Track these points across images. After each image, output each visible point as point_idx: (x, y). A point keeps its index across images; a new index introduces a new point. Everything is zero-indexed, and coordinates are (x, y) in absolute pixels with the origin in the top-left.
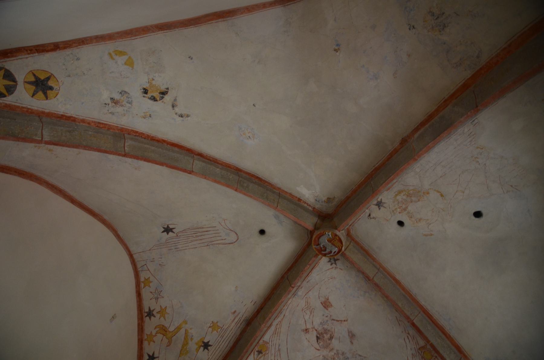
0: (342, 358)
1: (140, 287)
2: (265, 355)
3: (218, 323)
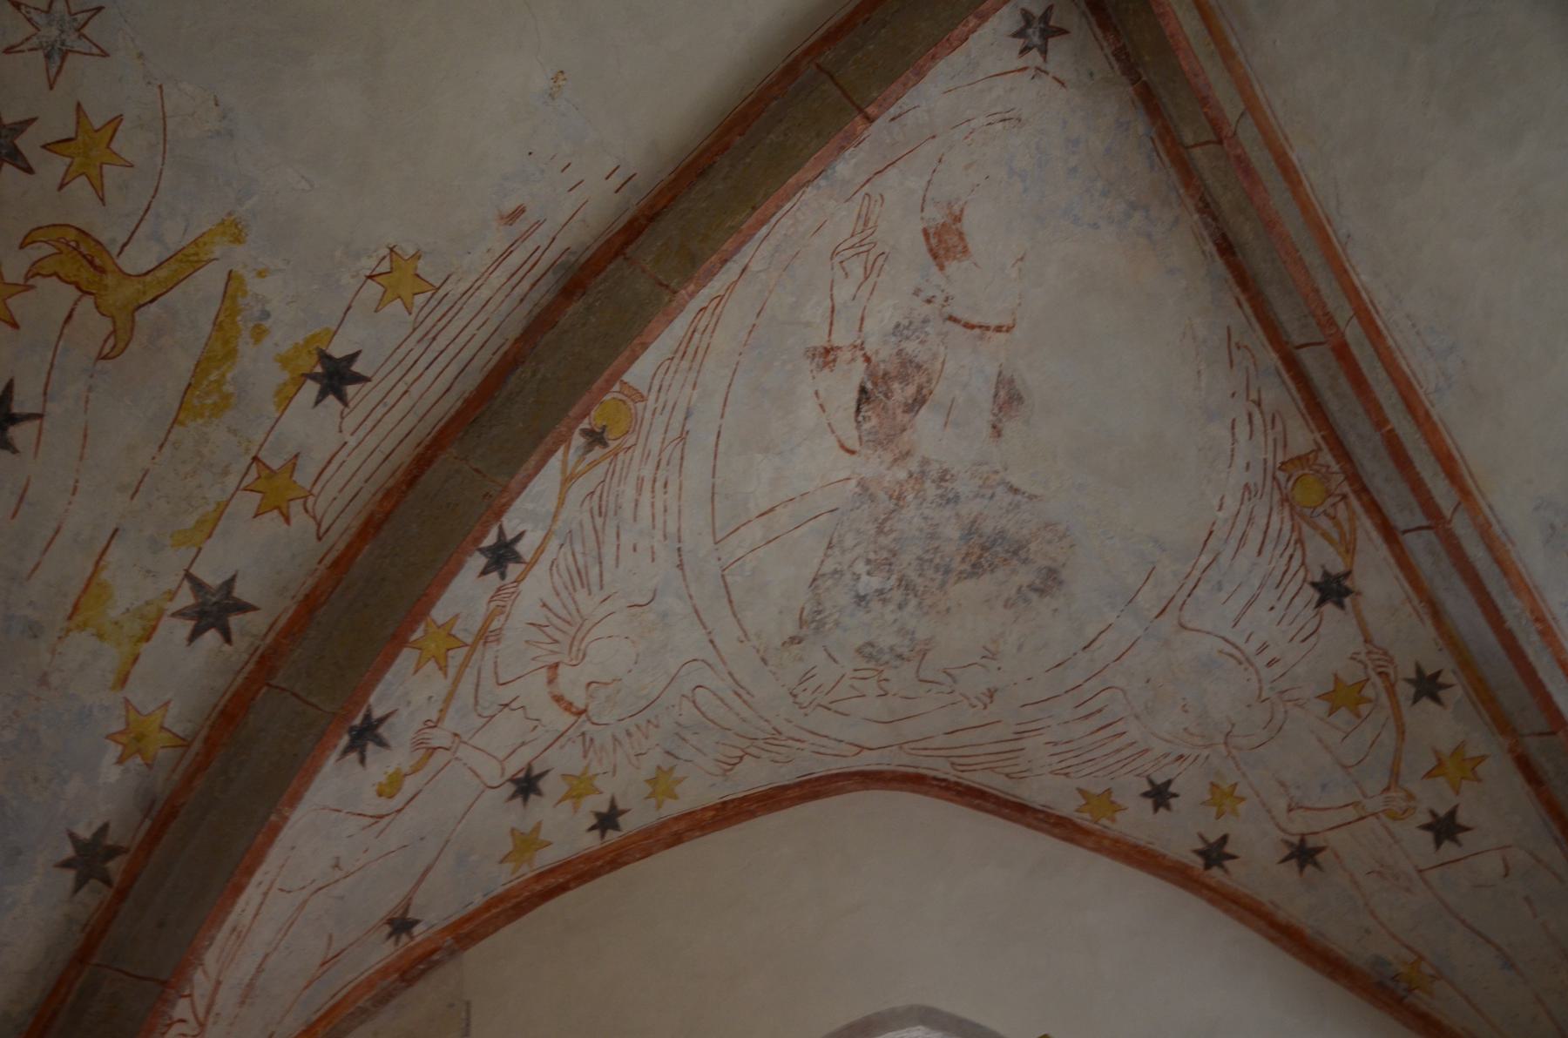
2: (616, 455)
3: (419, 258)
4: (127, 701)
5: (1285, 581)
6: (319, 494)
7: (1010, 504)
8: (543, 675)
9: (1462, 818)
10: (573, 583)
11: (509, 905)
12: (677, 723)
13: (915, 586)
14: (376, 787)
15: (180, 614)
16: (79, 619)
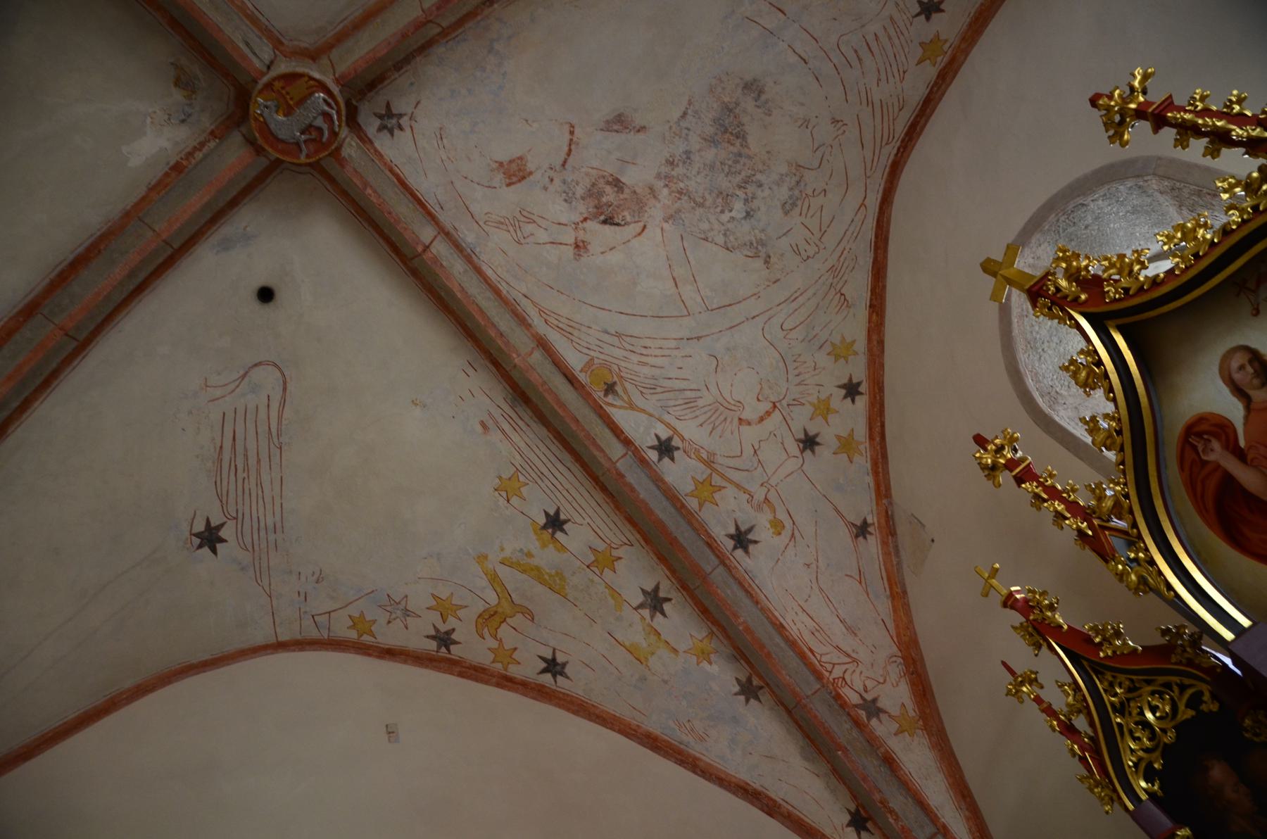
0: (685, 171)
1: (372, 646)
2: (622, 377)
4: (684, 652)
7: (694, 116)
8: (744, 428)
10: (692, 407)
11: (880, 460)
12: (802, 342)
13: (746, 177)
14: (774, 536)
15: (652, 617)
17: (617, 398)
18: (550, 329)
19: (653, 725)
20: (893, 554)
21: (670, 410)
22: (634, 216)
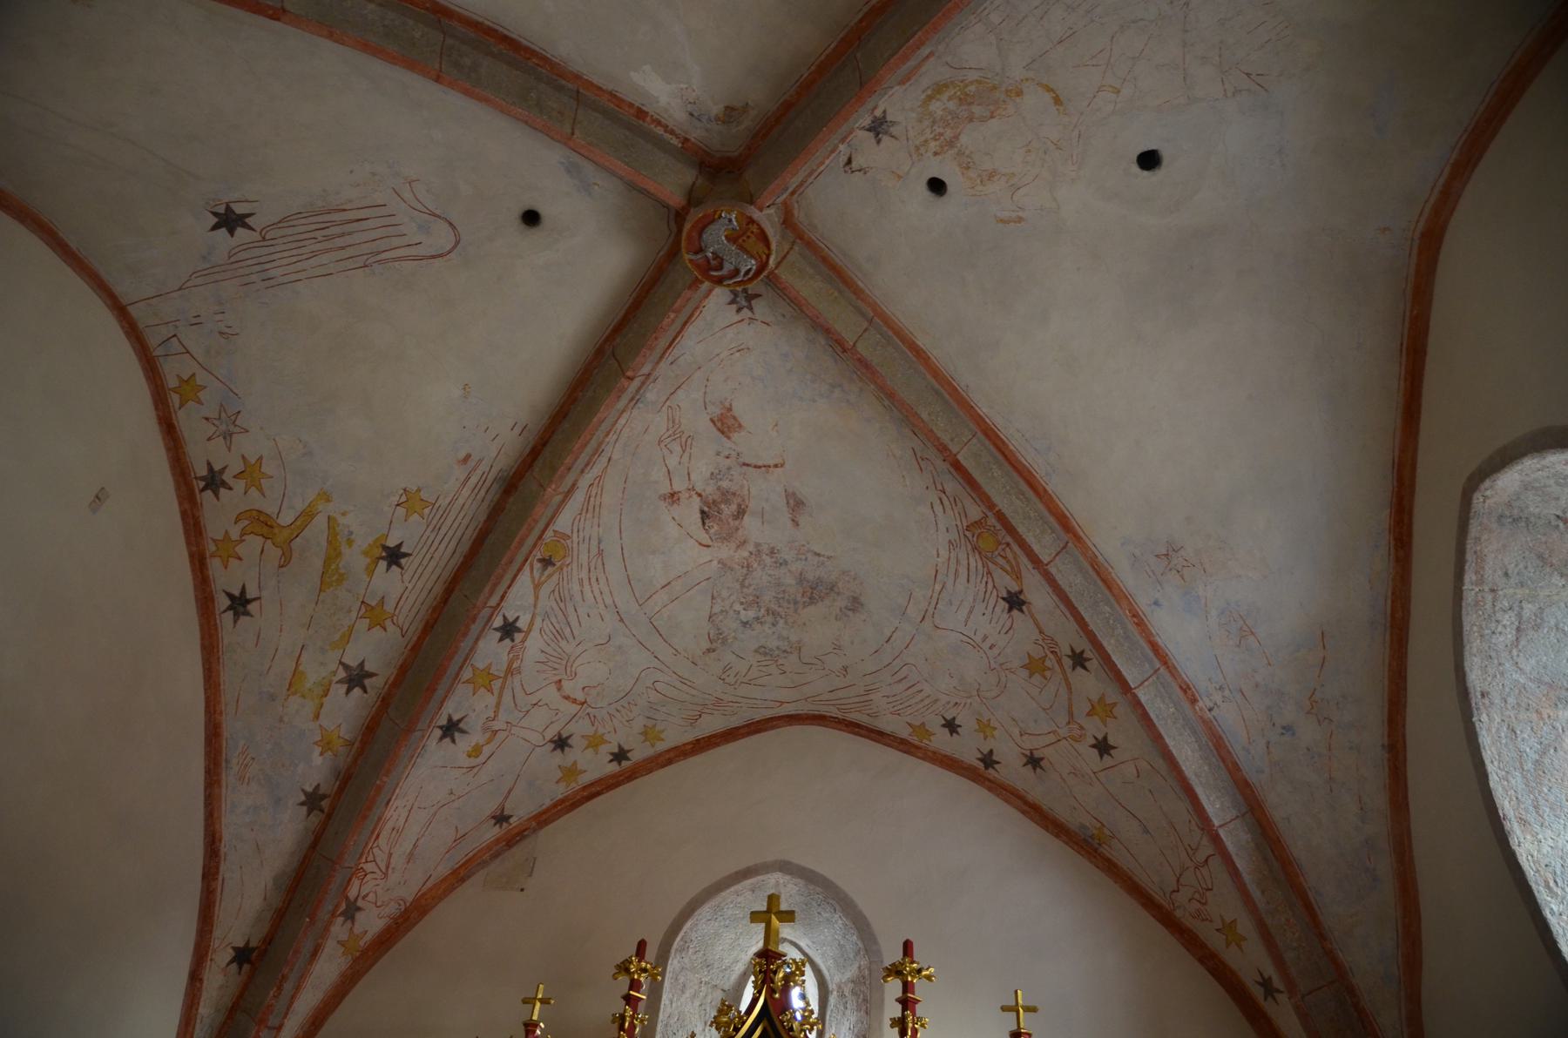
2: (562, 569)
3: (420, 491)
4: (321, 726)
5: (987, 598)
6: (399, 614)
8: (553, 688)
9: (1111, 741)
15: (340, 682)
16: (293, 689)
17: (540, 571)
18: (585, 491)
19: (231, 727)
20: (491, 852)
21: (547, 621)
22: (716, 535)
